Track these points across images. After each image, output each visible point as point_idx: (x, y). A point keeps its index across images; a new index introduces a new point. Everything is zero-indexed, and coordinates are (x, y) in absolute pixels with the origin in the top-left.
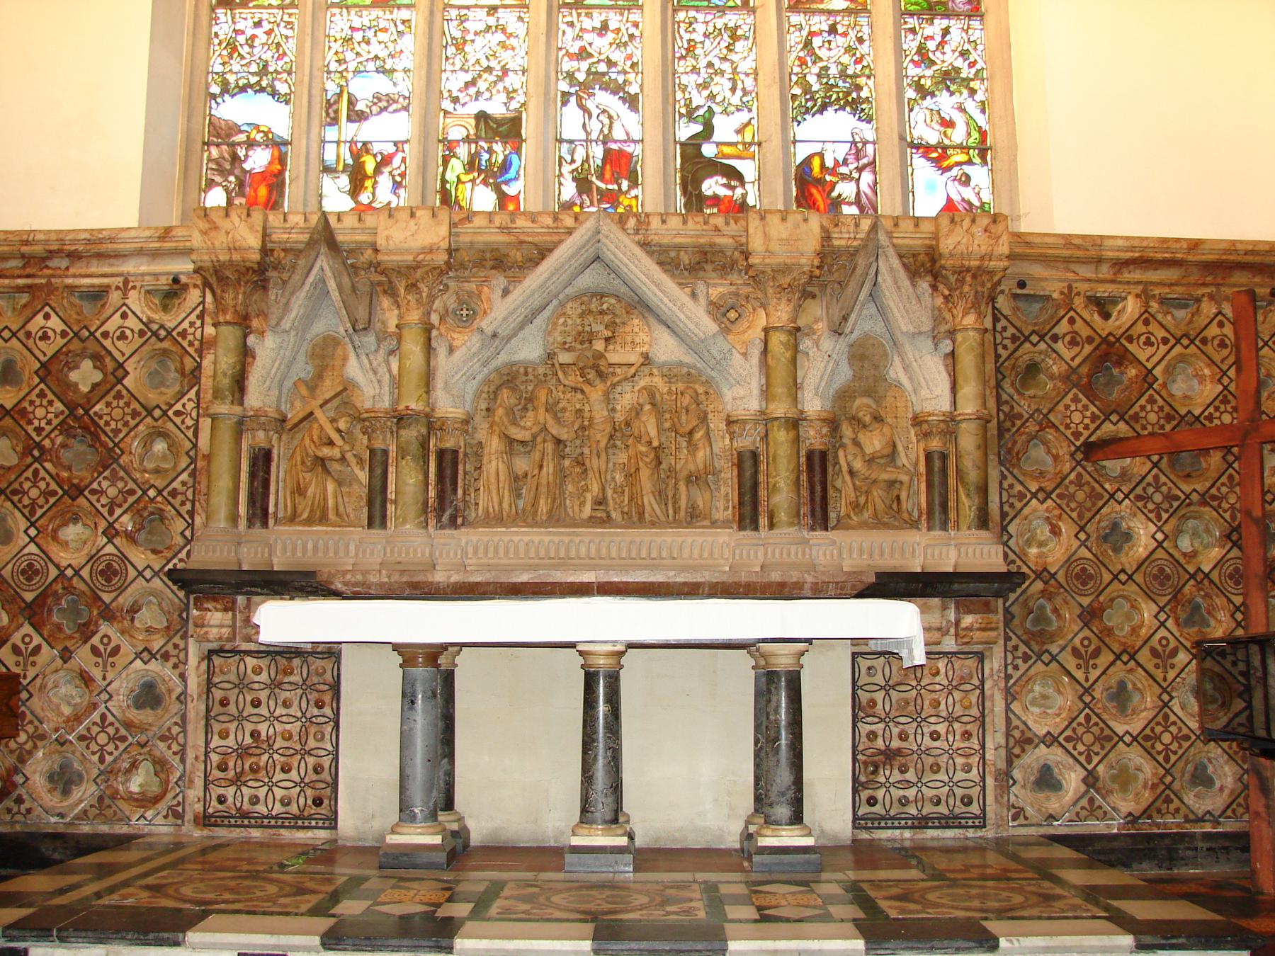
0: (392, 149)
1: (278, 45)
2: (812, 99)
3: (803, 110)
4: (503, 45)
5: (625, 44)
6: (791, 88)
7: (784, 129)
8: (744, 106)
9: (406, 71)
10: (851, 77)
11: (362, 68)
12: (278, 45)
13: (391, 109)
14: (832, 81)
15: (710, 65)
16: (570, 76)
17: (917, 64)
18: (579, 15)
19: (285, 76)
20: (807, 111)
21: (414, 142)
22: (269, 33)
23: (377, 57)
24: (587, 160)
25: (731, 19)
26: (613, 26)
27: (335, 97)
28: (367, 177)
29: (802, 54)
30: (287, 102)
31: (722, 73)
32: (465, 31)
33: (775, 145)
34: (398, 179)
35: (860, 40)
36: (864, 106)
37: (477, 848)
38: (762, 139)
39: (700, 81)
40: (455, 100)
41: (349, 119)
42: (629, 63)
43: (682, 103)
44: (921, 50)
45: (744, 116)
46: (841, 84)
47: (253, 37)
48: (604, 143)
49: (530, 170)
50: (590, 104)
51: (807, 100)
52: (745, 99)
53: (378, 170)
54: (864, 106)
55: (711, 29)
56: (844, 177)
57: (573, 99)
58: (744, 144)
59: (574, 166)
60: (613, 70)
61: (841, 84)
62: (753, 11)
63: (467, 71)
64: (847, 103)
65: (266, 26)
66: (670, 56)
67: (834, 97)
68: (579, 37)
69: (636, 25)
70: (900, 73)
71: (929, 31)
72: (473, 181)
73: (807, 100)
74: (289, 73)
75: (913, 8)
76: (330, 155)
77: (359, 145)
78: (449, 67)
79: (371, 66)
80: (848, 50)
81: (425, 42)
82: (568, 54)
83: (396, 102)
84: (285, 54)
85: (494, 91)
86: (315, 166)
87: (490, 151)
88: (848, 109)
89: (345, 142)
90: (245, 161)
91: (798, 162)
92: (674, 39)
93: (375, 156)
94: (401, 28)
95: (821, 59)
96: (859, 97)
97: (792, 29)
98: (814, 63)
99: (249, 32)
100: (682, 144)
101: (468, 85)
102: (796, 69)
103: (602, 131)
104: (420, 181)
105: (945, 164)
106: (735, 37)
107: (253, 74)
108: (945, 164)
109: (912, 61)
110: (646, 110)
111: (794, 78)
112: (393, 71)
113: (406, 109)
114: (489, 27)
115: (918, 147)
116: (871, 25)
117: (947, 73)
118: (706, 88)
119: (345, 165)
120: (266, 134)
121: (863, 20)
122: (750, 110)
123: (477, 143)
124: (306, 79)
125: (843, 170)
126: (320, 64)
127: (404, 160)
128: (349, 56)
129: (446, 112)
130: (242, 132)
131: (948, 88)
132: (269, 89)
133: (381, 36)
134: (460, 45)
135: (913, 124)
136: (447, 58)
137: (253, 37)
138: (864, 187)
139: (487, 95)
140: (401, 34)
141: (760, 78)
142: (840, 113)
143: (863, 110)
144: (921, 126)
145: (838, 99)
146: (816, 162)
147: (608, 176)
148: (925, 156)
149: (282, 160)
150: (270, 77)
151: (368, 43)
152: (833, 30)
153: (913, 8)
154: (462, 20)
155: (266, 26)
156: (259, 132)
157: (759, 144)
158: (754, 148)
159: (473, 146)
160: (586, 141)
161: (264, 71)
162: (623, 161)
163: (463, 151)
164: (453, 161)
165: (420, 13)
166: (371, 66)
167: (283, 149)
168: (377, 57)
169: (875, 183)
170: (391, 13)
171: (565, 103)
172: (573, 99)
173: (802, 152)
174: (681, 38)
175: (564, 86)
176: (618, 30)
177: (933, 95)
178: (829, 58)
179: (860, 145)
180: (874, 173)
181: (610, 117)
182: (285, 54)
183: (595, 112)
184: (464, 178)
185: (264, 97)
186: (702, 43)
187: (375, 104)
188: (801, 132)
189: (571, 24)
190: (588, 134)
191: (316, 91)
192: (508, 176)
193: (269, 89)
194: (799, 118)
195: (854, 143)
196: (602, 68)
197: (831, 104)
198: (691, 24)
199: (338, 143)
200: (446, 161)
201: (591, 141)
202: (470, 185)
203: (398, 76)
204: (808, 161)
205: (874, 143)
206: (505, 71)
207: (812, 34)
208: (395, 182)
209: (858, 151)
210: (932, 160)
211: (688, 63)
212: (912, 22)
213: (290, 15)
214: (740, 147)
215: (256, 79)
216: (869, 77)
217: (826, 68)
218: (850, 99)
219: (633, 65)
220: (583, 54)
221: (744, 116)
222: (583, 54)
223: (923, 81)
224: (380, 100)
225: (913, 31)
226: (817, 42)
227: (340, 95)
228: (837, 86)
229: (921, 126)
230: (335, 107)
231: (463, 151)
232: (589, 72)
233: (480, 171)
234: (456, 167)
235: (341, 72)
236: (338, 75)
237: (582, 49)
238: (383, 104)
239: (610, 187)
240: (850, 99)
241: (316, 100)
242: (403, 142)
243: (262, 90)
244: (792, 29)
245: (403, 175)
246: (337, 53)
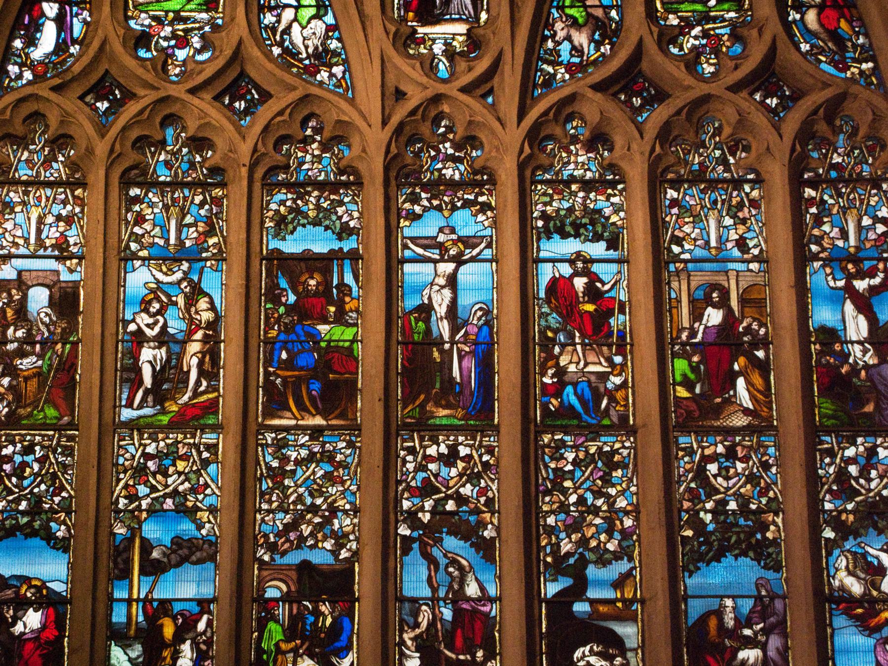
0: (196, 609)
1: (54, 476)
2: (707, 542)
3: (696, 556)
4: (328, 476)
5: (479, 476)
6: (681, 528)
7: (673, 581)
8: (623, 553)
9: (212, 510)
10: (754, 512)
11: (158, 507)
12: (54, 476)
13: (194, 558)
14: (731, 519)
15: (581, 500)
16: (412, 517)
17: (835, 495)
18: (422, 439)
19: (63, 515)
20: (702, 558)
21: (225, 601)
22: (42, 461)
23: (176, 492)
24: (432, 624)
25: (608, 443)
26: (463, 451)
27: (125, 543)
28: (165, 645)
29: (693, 485)
30: (66, 550)
31: (596, 511)
32: (285, 460)
33: (661, 604)
34: (203, 647)
35: (766, 466)
36: (770, 550)
37: (570, 576)
38: (647, 596)
39: (570, 521)
40: (272, 548)
41: (143, 572)
42: (483, 500)
43: (548, 550)
44: (842, 476)
45: (623, 566)
46: (742, 521)
47: (24, 465)
48: (454, 602)
49: (366, 635)
50: (436, 552)
51: (700, 544)
52: (625, 544)
53: (179, 638)
54: (770, 550)
55: (581, 455)
56: (750, 643)
57: (416, 546)
58: (623, 600)
59: (418, 631)
60: (464, 508)
61: (742, 521)
62: (632, 431)
63: (286, 512)
64: (750, 547)
65: (39, 452)
66: (533, 489)
67: (734, 539)
68: (424, 468)
69: (490, 451)
70: (814, 504)
71: (850, 452)
72: (295, 651)
73: (700, 544)
74: (68, 513)
75: (830, 422)
76: (119, 615)
77: (155, 604)
78: (265, 506)
79: (169, 503)
80: (752, 479)
81: (237, 475)
82: (409, 488)
83: (201, 549)
84: (62, 488)
85: (320, 536)
86: (101, 631)
87: (317, 613)
88: (751, 554)
89: (138, 600)
90: (14, 624)
91: (691, 622)
92: (537, 470)
93: (174, 618)
94: (205, 455)
95: (718, 492)
96: (765, 538)
97: (681, 453)
98: (709, 497)
99: (18, 459)
100: (548, 602)
101: (288, 528)
102: (686, 505)
103: (451, 587)
104: (233, 653)
105: (874, 622)
106: (612, 466)
107: (23, 513)
108: (874, 622)
109: (830, 491)
110: (506, 563)
111: (685, 517)
112: (196, 509)
113: (212, 558)
114: (312, 455)
115: (838, 601)
116: (778, 447)
117: (874, 504)
118: (576, 531)
119: (138, 629)
120: (39, 589)
121: (768, 441)
122: (631, 559)
123: (299, 603)
124: (92, 523)
125: (747, 632)
126: (108, 502)
127: (209, 623)
128: (143, 490)
129: (261, 562)
130: (10, 587)
131: (876, 527)
132: (42, 532)
133: (181, 465)
134: (278, 475)
135: (832, 572)
136: (262, 494)
137: (24, 465)
138: (772, 653)
139: (311, 542)
140: (206, 463)
141: (643, 517)
142: (742, 560)
143: (770, 555)
144: (842, 574)
145: (739, 542)
146: (713, 623)
147: (459, 642)
148: (848, 614)
149: (60, 624)
150: (44, 516)
151: (166, 475)
152: (731, 454)
153: (830, 422)
154: (280, 445)
155: (39, 452)
156: (30, 587)
157: (643, 602)
158: (637, 607)
159: (295, 607)
160: (432, 599)
161: (35, 509)
162: (478, 625)
163: (282, 611)
164: (272, 626)
165: (230, 436)
166: (169, 503)
167: (60, 608)
168: (176, 492)
169: (786, 648)
170: (193, 436)
171: (406, 551)
172: (416, 546)
173: (696, 609)
174: (546, 466)
175: (404, 531)
176: (469, 457)
177: (857, 535)
178: (728, 489)
179: (766, 600)
180: (785, 635)
181: (461, 568)
182: (62, 488)
183: (443, 561)
184: (283, 646)
185: (36, 542)
186: (572, 472)
187: (174, 552)
188: (693, 582)
189: (412, 451)
190: (434, 590)
191: (103, 537)
192: (338, 644)
193: (42, 532)
194: (691, 567)
195: (758, 598)
196: (450, 506)
197: (730, 549)
198: (558, 448)
199: (129, 601)
200: (261, 628)
201: (438, 599)
202: (290, 656)
203: (204, 516)
204: (704, 619)
205: (784, 597)
206: (334, 511)
207: (708, 459)
208: (199, 650)
209: (765, 607)
210: (857, 618)
211: (555, 498)
212: (829, 441)
213: (71, 438)
214: (619, 605)
215: (24, 520)
216: (776, 514)
217: (724, 503)
218: (753, 541)
219: (489, 502)
220: (427, 489)
221: (623, 566)
222: (427, 489)
223: (844, 517)
224: (180, 546)
225: (831, 453)
226: (713, 468)
227: (130, 540)
228: (737, 525)
229: (842, 574)
230: (125, 556)
231: (282, 611)
232: (433, 512)
233: (304, 639)
234: (275, 631)
235: (132, 511)
236: (128, 515)
237: (426, 481)
238: (184, 552)
239: (462, 657)
240: (753, 541)
241: (104, 548)
242: (210, 601)
243: (34, 534)
244: (681, 453)
245: (209, 643)
246: (126, 486)
